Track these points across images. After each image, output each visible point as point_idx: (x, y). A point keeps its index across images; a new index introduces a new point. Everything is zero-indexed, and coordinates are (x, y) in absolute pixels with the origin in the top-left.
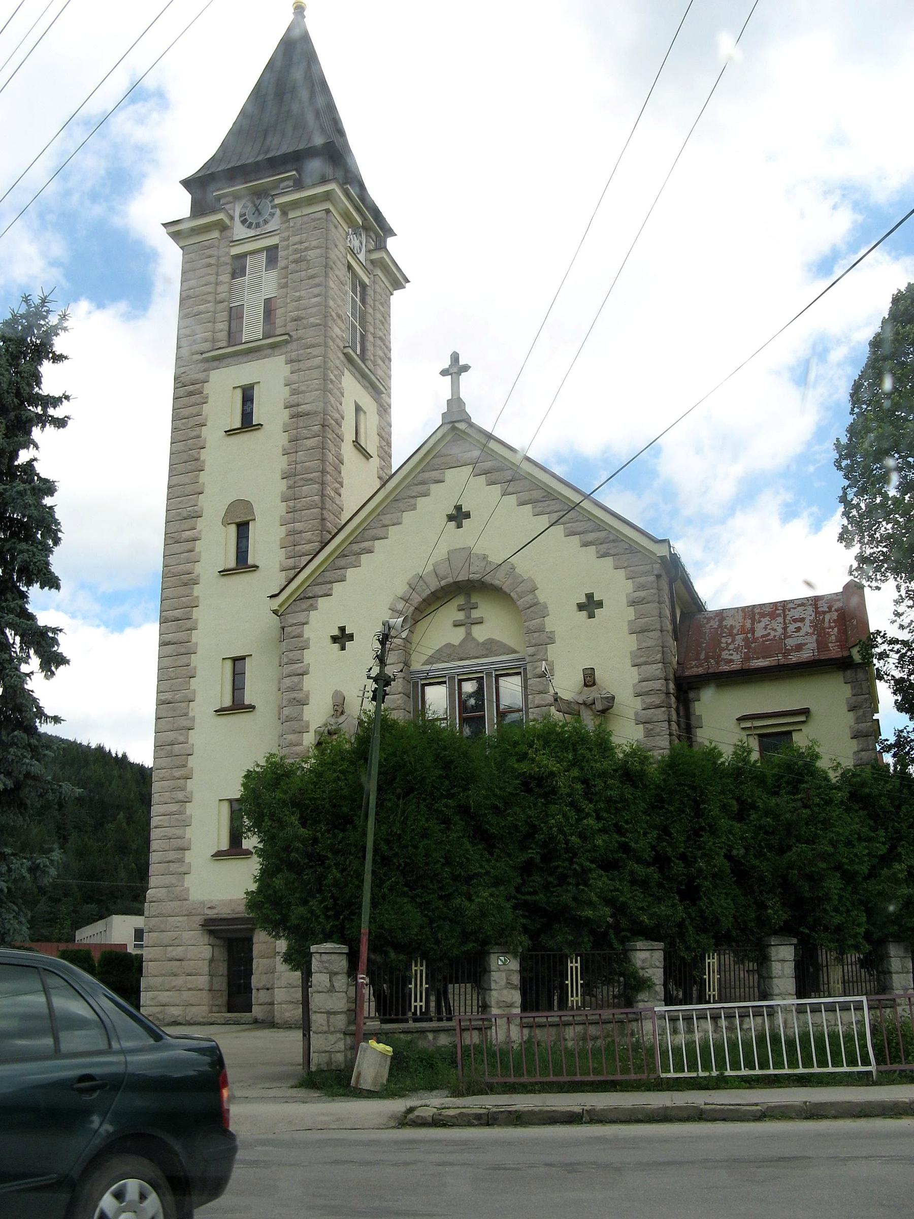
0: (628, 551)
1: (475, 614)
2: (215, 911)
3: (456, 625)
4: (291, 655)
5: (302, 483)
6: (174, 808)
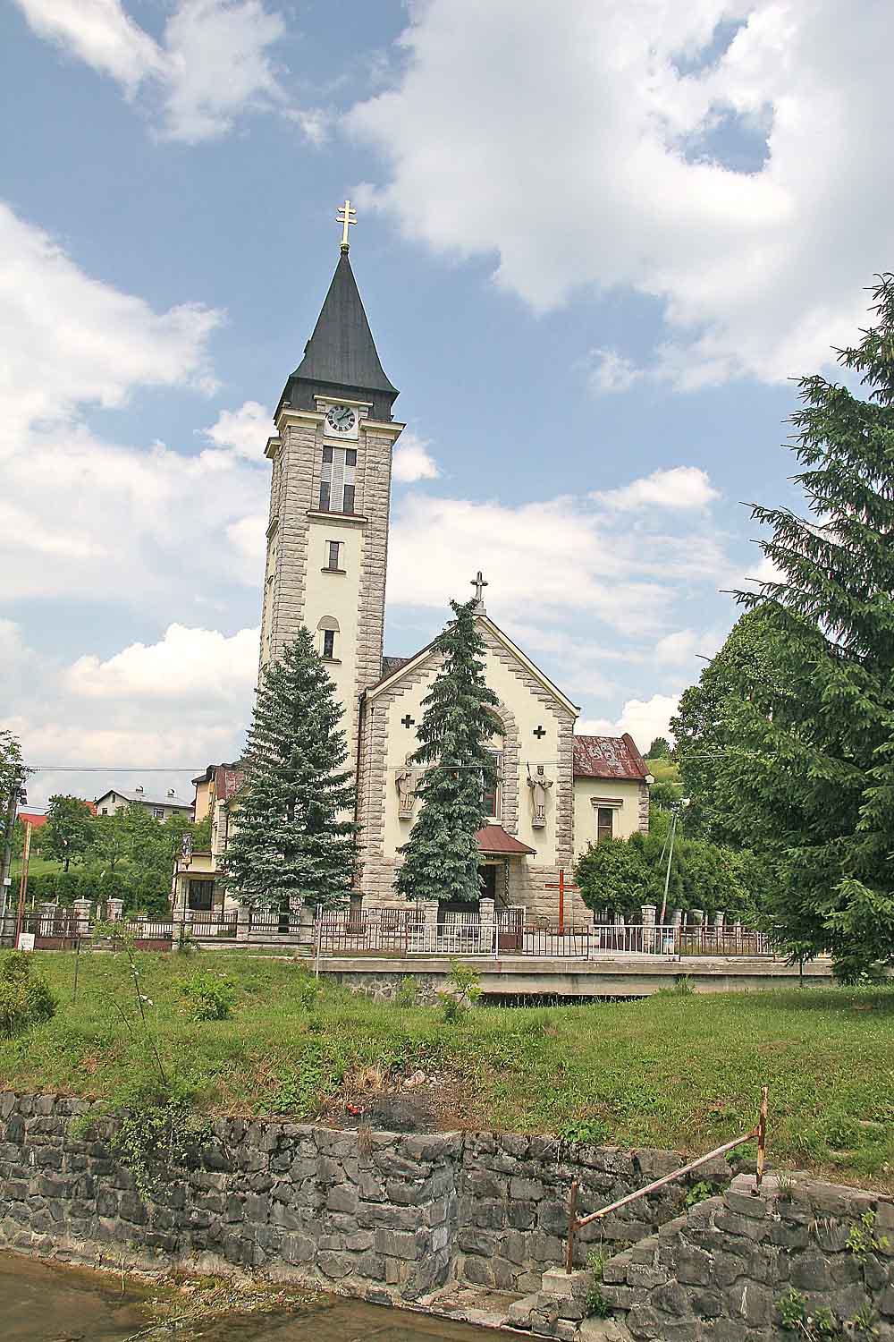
5: (371, 617)
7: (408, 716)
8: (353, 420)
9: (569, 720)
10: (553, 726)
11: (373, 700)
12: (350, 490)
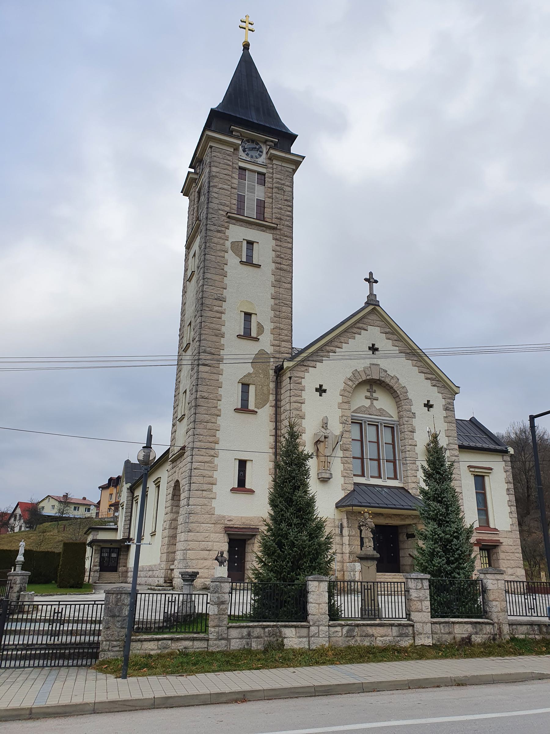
0: (443, 387)
1: (375, 395)
2: (232, 523)
3: (367, 398)
4: (296, 392)
5: (282, 304)
6: (208, 459)
7: (373, 345)
8: (262, 152)
9: (451, 396)
10: (438, 401)
11: (292, 369)
12: (261, 205)
